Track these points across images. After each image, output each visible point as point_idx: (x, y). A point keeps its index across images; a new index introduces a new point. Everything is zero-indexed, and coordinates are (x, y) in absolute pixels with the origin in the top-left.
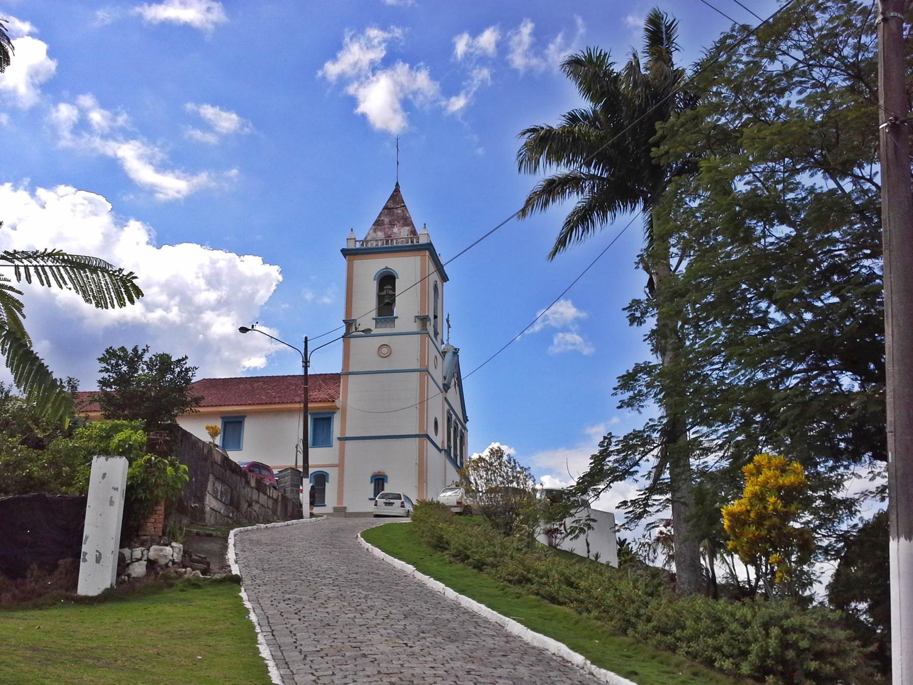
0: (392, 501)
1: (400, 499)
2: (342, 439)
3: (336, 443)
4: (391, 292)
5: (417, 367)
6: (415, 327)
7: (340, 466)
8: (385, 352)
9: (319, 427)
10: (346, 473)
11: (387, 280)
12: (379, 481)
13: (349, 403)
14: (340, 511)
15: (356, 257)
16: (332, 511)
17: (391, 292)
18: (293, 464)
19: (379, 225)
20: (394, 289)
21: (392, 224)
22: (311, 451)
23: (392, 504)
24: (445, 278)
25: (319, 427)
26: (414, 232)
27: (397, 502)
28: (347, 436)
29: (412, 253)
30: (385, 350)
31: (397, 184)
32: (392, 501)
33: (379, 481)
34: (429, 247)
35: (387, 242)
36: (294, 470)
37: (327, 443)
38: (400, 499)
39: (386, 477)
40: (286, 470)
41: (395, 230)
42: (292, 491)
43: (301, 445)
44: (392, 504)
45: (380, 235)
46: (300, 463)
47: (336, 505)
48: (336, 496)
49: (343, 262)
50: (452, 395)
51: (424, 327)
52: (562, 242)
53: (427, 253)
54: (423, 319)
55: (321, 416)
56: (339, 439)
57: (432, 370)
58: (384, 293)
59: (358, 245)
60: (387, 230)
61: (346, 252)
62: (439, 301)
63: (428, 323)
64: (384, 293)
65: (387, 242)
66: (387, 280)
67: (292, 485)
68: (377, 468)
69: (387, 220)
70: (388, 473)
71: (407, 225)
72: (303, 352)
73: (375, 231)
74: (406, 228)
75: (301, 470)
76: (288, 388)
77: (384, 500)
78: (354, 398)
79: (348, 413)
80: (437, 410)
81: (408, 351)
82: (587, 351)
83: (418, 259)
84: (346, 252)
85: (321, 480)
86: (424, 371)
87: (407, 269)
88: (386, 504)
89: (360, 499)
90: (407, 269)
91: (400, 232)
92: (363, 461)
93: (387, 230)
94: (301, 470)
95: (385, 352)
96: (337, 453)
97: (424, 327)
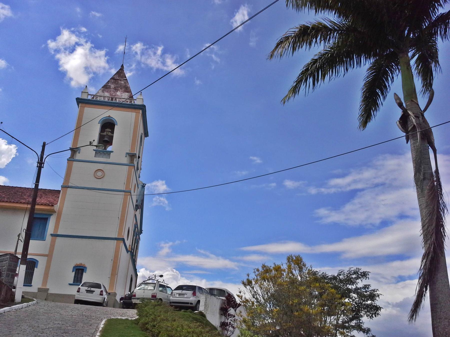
0: (92, 289)
1: (101, 288)
2: (55, 236)
3: (48, 238)
4: (110, 134)
5: (123, 188)
6: (126, 160)
7: (49, 256)
8: (99, 175)
9: (37, 224)
10: (53, 262)
11: (108, 126)
12: (79, 271)
13: (64, 209)
14: (43, 291)
15: (87, 105)
16: (36, 291)
17: (110, 134)
18: (12, 251)
19: (107, 88)
20: (113, 132)
21: (116, 89)
22: (31, 242)
23: (92, 292)
24: (146, 134)
25: (37, 224)
26: (131, 97)
27: (97, 291)
28: (59, 233)
29: (130, 110)
30: (99, 174)
31: (122, 66)
32: (92, 289)
33: (79, 271)
34: (143, 108)
35: (112, 99)
36: (13, 257)
37: (42, 237)
38: (101, 288)
39: (86, 268)
40: (7, 254)
41: (118, 93)
42: (8, 276)
43: (23, 235)
44: (92, 292)
45: (107, 94)
46: (20, 250)
47: (40, 286)
48: (42, 279)
49: (75, 108)
50: (138, 212)
51: (132, 161)
52: (295, 90)
53: (141, 111)
54: (132, 156)
55: (41, 216)
56: (52, 235)
57: (132, 192)
58: (105, 134)
59: (90, 97)
60: (112, 92)
61: (79, 101)
62: (142, 147)
63: (135, 159)
64: (105, 134)
65: (112, 99)
66: (108, 126)
67: (9, 270)
68: (78, 262)
69: (112, 86)
70: (87, 265)
71: (127, 92)
72: (39, 154)
73: (103, 91)
74: (127, 94)
75: (20, 256)
76: (15, 193)
77: (86, 288)
78: (67, 205)
79: (62, 218)
80: (130, 224)
81: (118, 177)
82: (167, 209)
83: (134, 114)
84: (79, 101)
85: (31, 265)
86: (127, 192)
87: (124, 119)
88: (88, 291)
89: (63, 285)
90: (124, 119)
91: (122, 96)
92: (70, 254)
93: (112, 92)
94: (20, 256)
95: (99, 175)
96: (49, 246)
97: (132, 161)
